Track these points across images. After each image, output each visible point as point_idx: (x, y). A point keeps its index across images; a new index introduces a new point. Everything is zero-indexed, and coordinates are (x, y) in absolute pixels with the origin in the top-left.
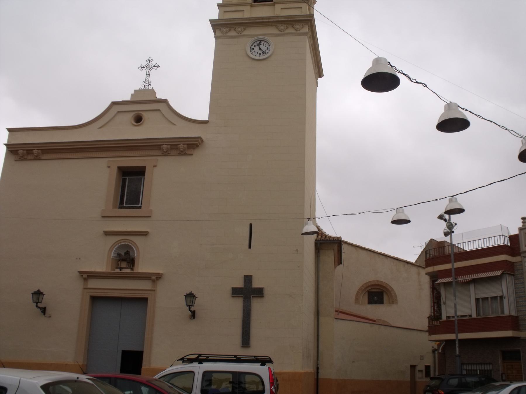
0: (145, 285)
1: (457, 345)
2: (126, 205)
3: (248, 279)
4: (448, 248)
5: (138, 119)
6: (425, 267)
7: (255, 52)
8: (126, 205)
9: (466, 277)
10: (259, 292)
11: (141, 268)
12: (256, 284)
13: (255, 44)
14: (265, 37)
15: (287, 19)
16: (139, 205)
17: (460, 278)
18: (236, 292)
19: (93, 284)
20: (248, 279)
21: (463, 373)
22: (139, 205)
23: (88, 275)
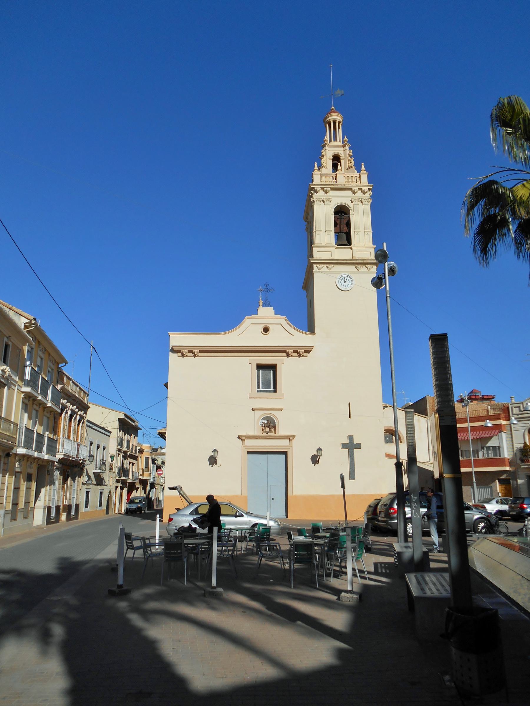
0: (286, 442)
1: (474, 476)
2: (262, 389)
3: (351, 438)
4: (408, 419)
5: (266, 330)
6: (92, 458)
7: (342, 284)
8: (262, 389)
9: (490, 433)
10: (358, 446)
11: (281, 431)
12: (346, 441)
13: (343, 277)
14: (350, 275)
15: (362, 262)
16: (271, 389)
17: (490, 433)
18: (344, 446)
19: (248, 442)
20: (351, 438)
21: (489, 489)
22: (271, 389)
23: (246, 437)
